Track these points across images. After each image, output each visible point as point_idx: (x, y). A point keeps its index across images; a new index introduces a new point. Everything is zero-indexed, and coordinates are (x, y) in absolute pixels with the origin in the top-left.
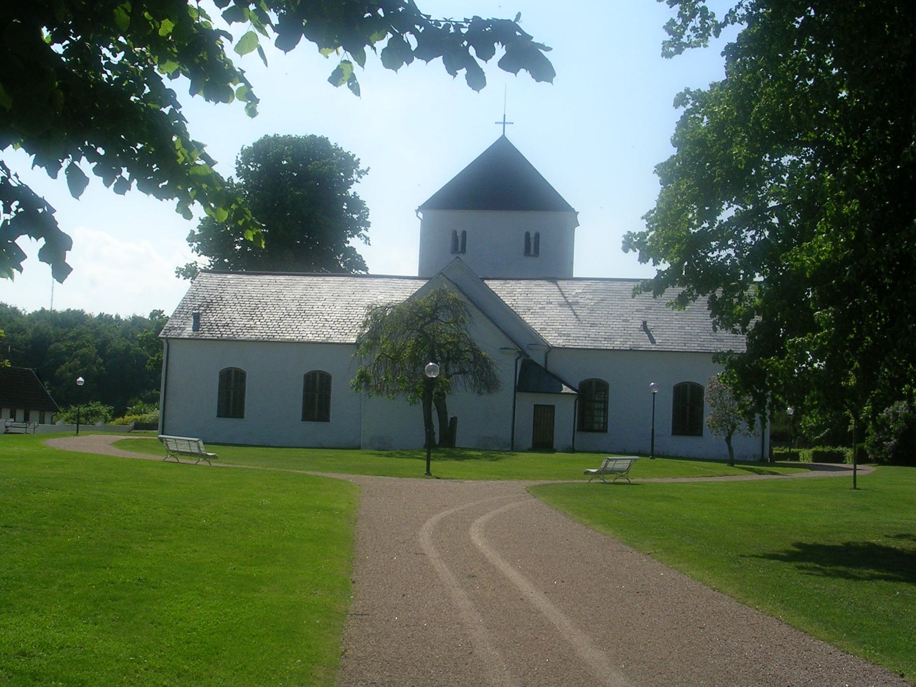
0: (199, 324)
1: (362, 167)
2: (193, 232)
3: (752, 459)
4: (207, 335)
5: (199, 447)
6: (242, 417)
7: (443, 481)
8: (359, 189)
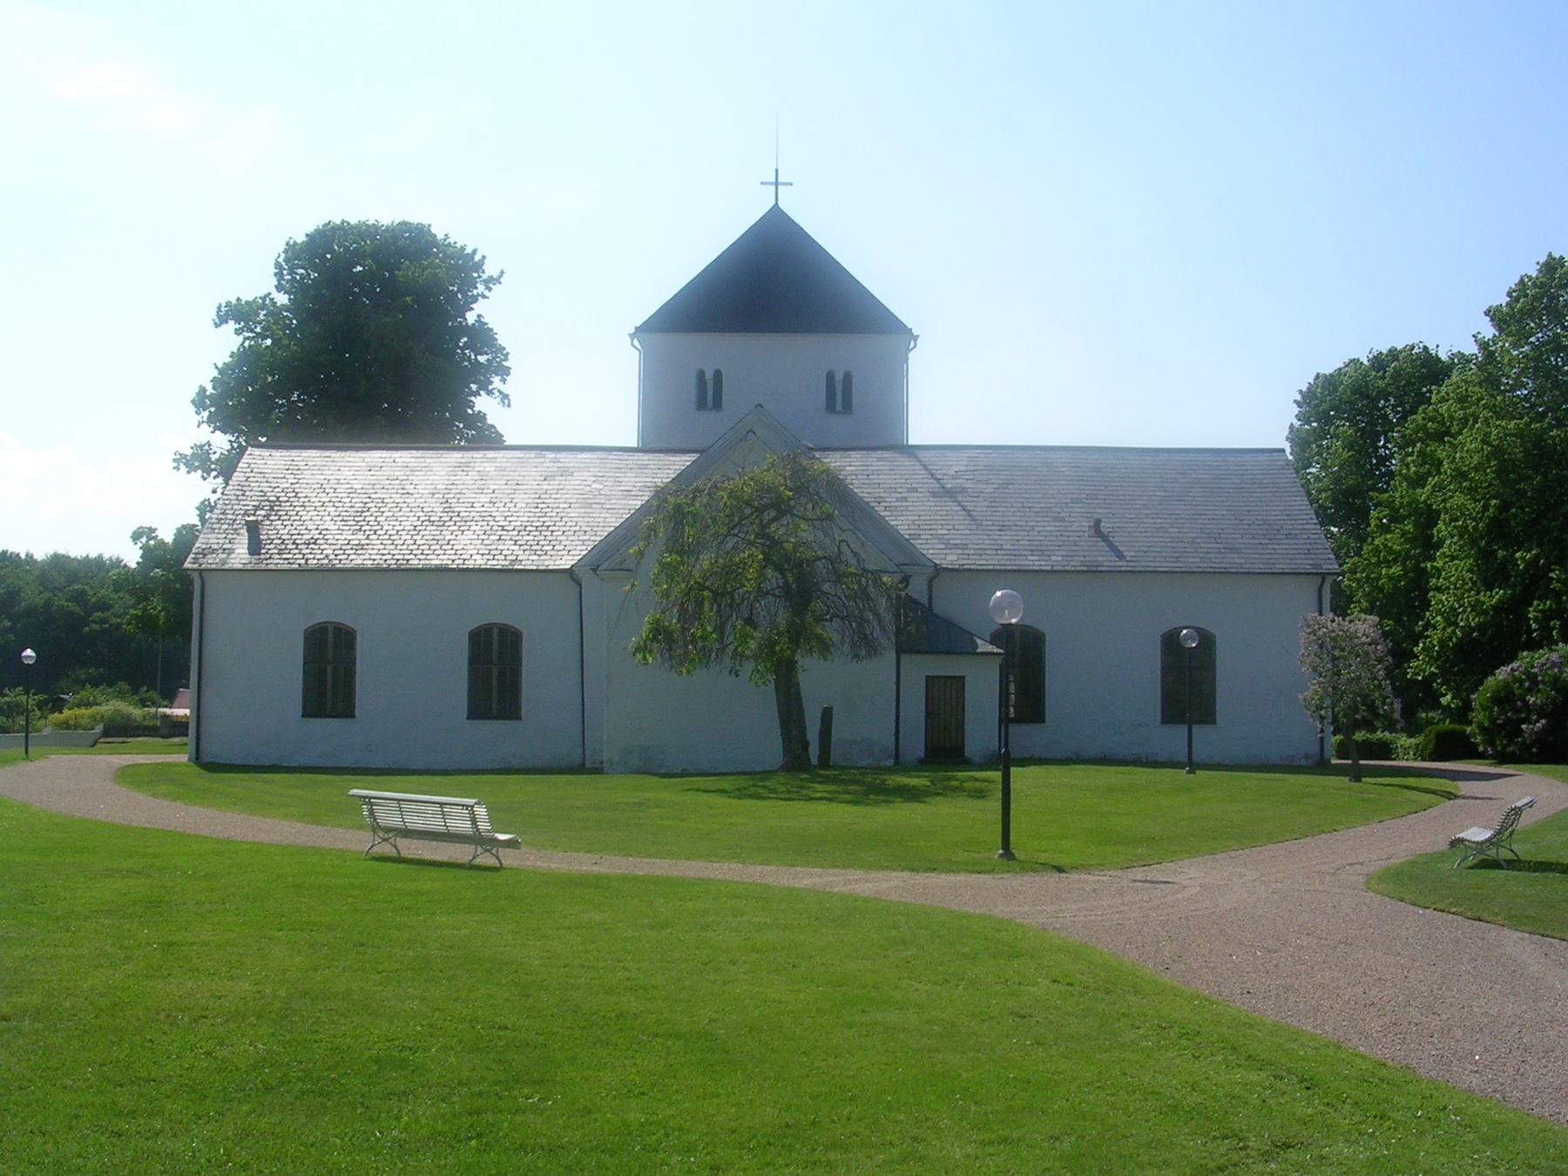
0: (260, 541)
1: (490, 270)
2: (203, 390)
3: (1303, 762)
4: (277, 562)
5: (474, 821)
6: (353, 716)
7: (1074, 876)
8: (487, 310)
